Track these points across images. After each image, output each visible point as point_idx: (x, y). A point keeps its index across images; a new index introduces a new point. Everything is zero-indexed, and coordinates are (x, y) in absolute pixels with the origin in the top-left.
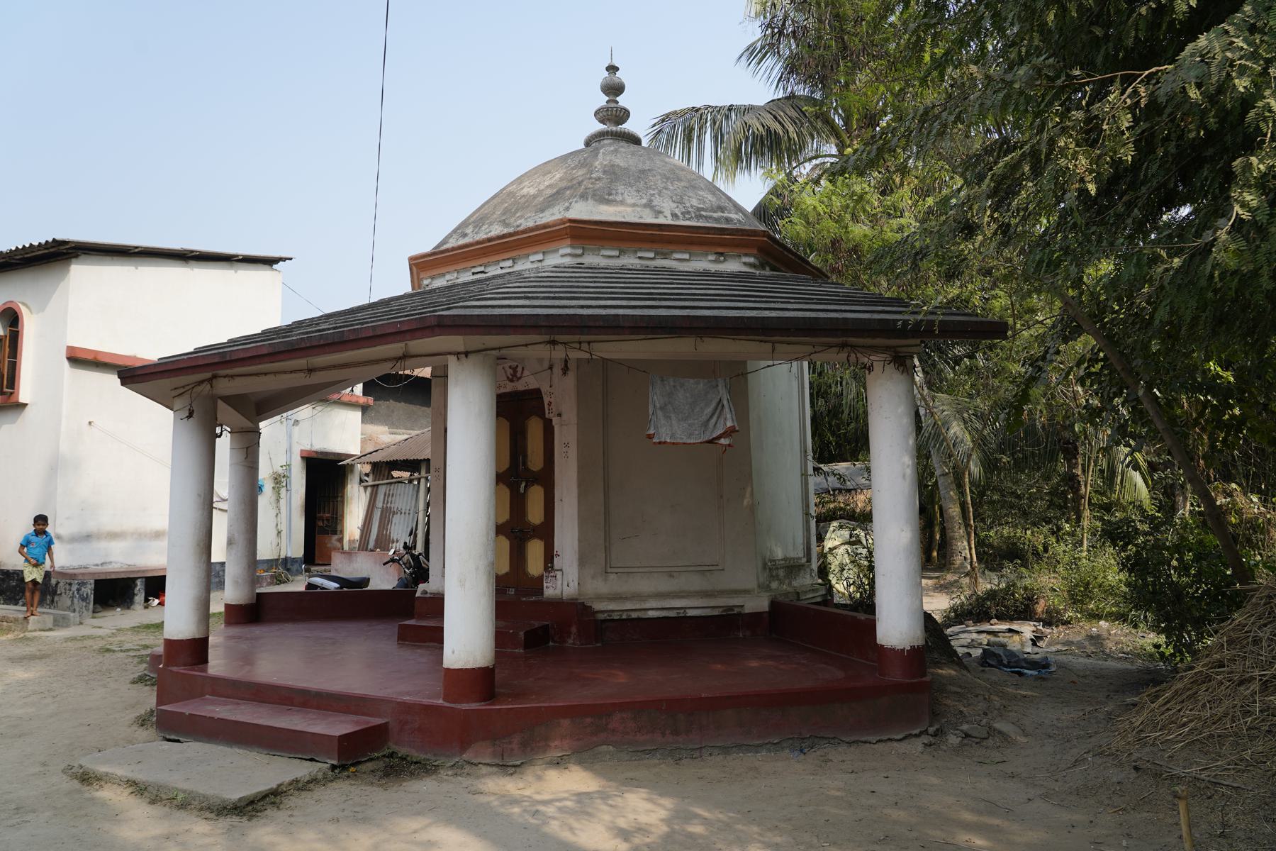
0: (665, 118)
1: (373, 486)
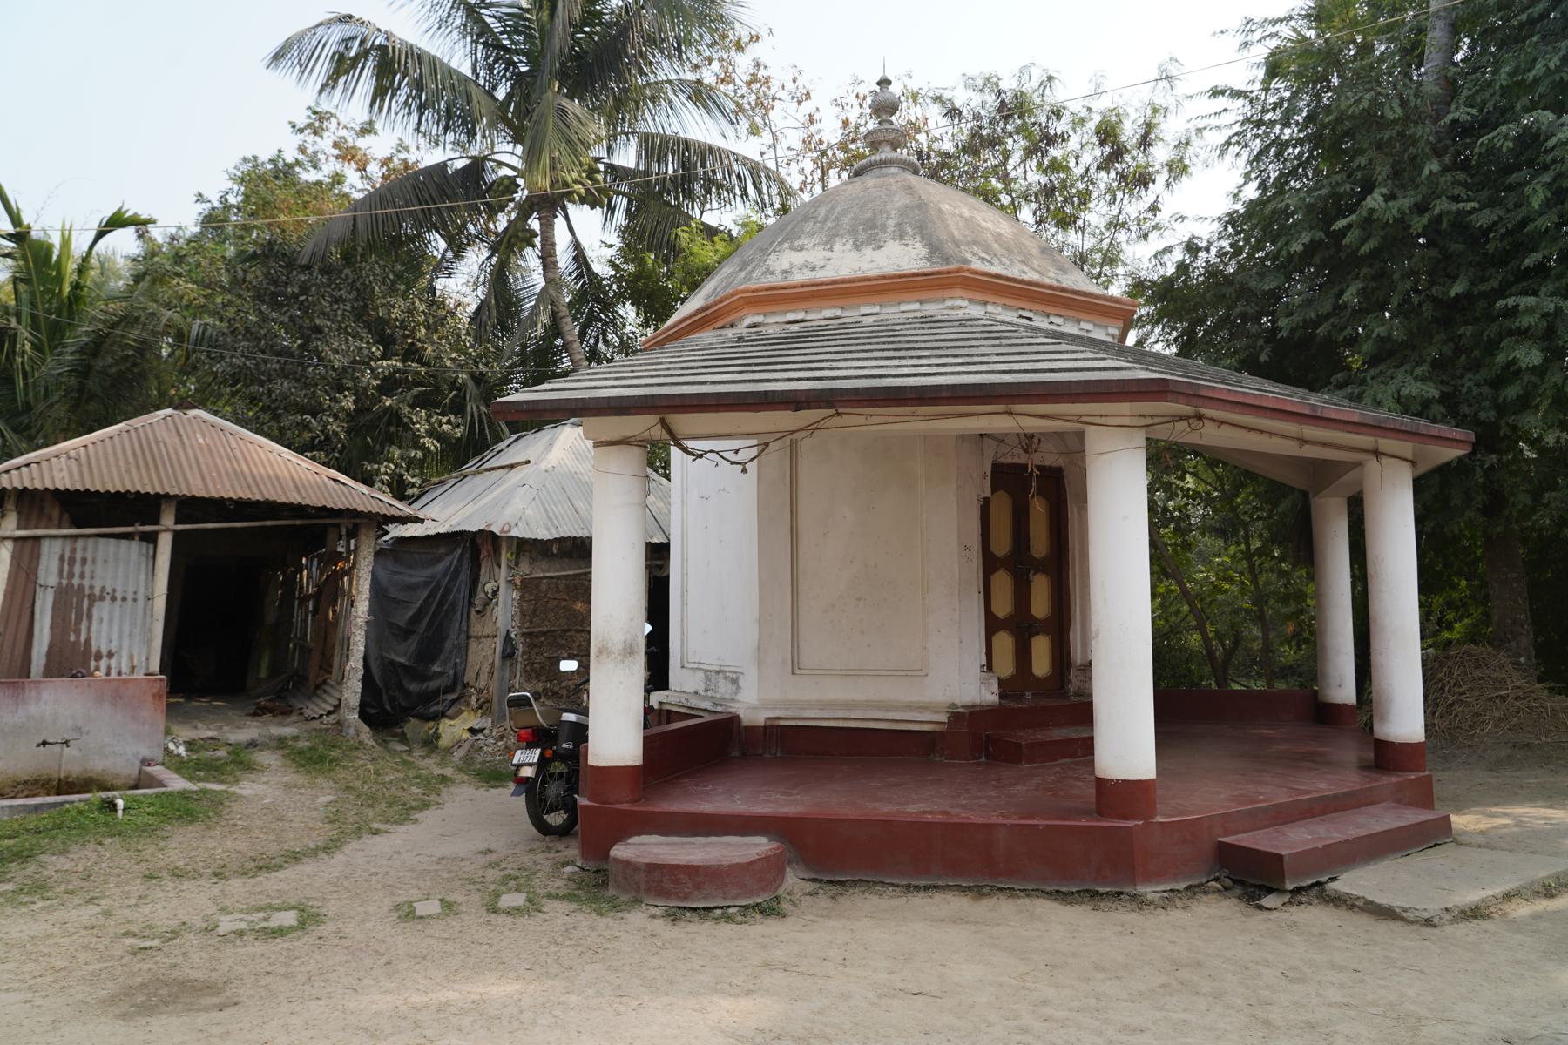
0: (348, 18)
1: (16, 539)
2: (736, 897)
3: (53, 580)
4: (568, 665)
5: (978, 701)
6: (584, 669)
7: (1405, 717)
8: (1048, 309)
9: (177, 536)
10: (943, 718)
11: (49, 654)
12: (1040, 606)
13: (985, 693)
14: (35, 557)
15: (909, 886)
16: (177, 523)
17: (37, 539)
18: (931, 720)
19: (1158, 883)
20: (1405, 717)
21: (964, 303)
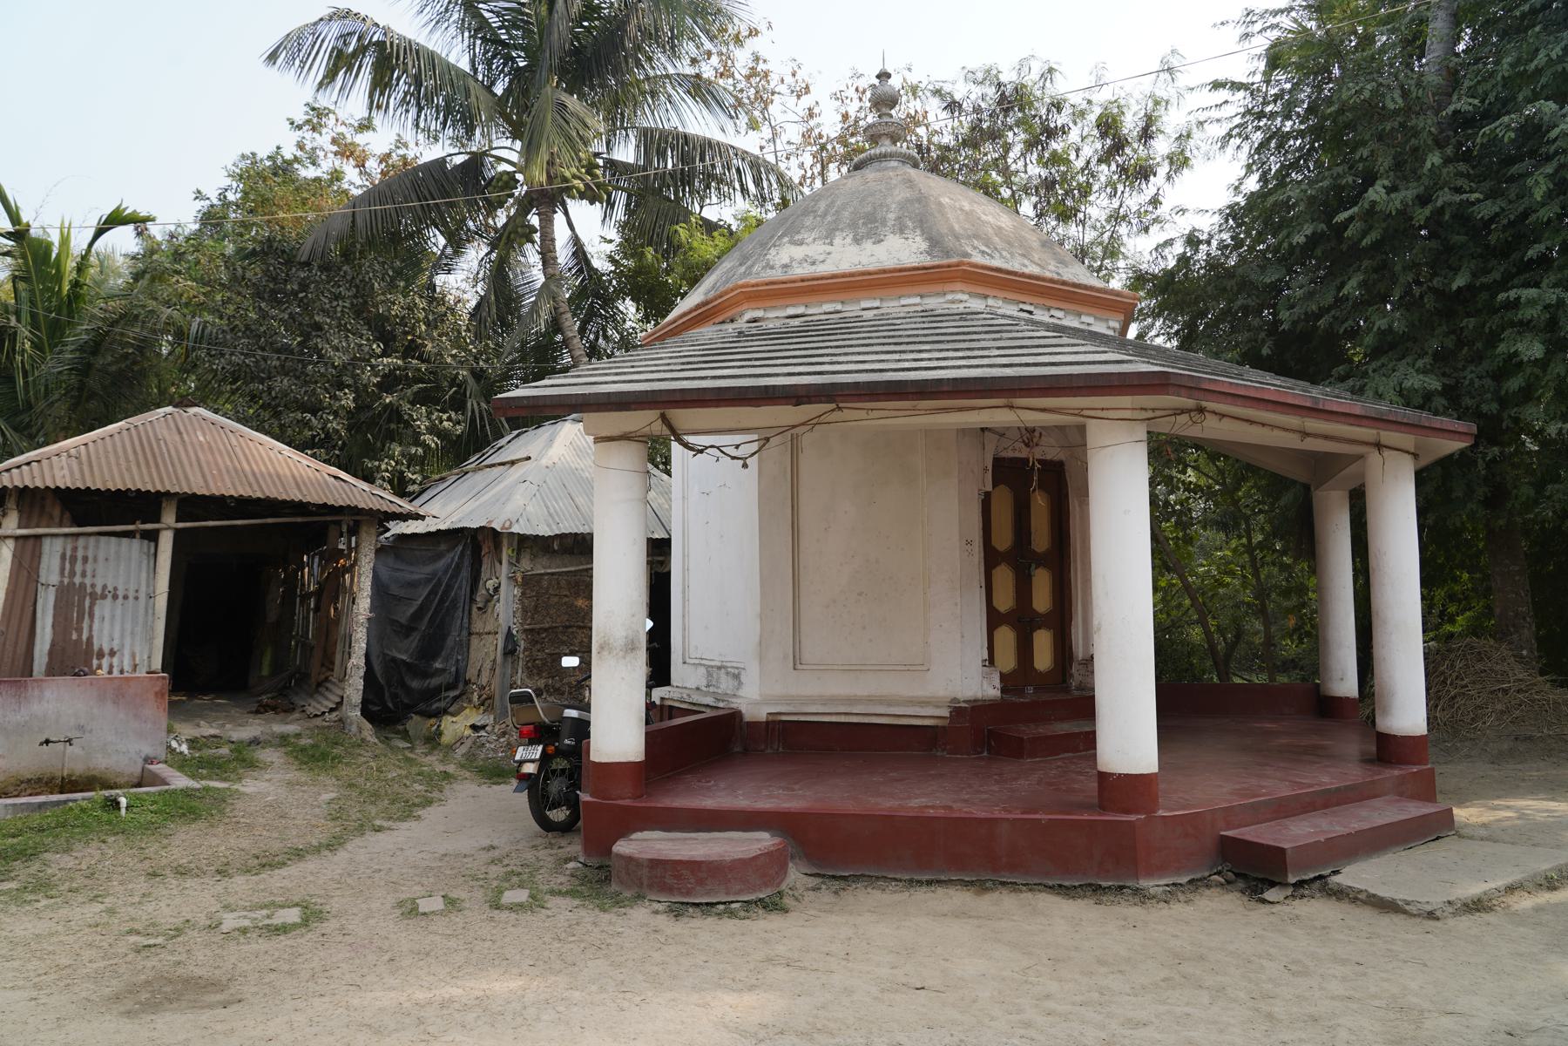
0: (347, 14)
2: (739, 892)
3: (54, 579)
4: (570, 662)
5: (979, 695)
6: (586, 665)
7: (1408, 710)
8: (1049, 303)
9: (178, 534)
10: (945, 713)
11: (51, 653)
12: (1042, 600)
13: (984, 687)
14: (37, 556)
15: (911, 881)
16: (177, 521)
17: (38, 537)
18: (931, 714)
19: (1161, 877)
20: (1408, 710)
21: (965, 297)
